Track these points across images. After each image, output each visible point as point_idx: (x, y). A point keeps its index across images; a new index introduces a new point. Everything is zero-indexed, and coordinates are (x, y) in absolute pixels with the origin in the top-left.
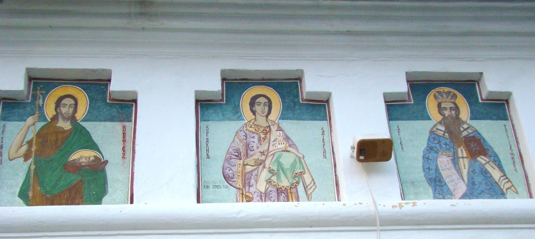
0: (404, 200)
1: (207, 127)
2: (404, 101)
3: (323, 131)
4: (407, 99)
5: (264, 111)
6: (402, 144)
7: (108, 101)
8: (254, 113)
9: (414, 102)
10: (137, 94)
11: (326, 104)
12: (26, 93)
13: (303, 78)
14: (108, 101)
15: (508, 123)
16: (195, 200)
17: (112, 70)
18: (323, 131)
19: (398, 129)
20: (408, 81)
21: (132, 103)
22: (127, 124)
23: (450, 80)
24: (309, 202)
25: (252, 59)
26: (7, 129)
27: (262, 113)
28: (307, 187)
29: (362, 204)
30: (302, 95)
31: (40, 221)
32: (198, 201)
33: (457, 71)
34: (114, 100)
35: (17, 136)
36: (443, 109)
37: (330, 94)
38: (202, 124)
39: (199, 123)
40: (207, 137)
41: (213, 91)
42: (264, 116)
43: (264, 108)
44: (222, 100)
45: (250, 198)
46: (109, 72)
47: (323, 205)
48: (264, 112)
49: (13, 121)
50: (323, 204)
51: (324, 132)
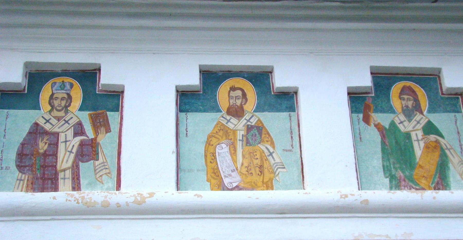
0: (361, 190)
1: (7, 113)
3: (187, 116)
7: (97, 93)
12: (199, 85)
13: (441, 71)
14: (97, 93)
18: (7, 115)
19: (358, 119)
20: (372, 73)
22: (292, 113)
25: (347, 55)
26: (71, 114)
28: (96, 167)
29: (310, 194)
35: (419, 126)
36: (402, 98)
40: (187, 123)
41: (10, 83)
47: (298, 194)
50: (299, 193)
51: (359, 119)
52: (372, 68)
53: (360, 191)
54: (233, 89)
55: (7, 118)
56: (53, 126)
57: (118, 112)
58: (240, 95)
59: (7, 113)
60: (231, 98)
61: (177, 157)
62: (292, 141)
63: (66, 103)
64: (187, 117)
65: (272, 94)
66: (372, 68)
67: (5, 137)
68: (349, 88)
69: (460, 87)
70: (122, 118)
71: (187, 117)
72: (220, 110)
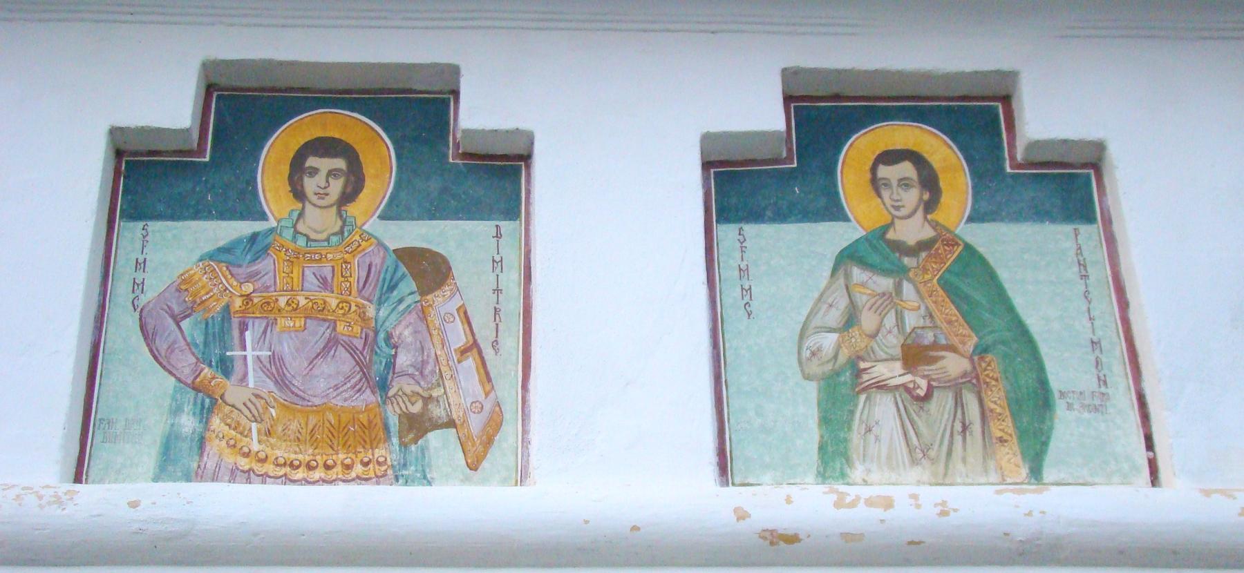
1: (143, 229)
2: (776, 161)
4: (784, 155)
5: (328, 190)
6: (1090, 296)
7: (795, 165)
8: (299, 194)
9: (211, 157)
10: (534, 138)
11: (523, 163)
12: (195, 135)
14: (795, 165)
15: (1090, 233)
16: (711, 469)
17: (463, 72)
21: (1087, 171)
22: (506, 226)
23: (929, 95)
24: (378, 486)
27: (316, 197)
30: (1012, 145)
31: (255, 535)
32: (78, 479)
33: (312, 59)
34: (468, 156)
37: (530, 138)
38: (130, 233)
39: (114, 222)
42: (331, 206)
43: (327, 181)
44: (201, 151)
45: (358, 469)
46: (453, 72)
48: (327, 195)
49: (186, 220)
52: (789, 75)
53: (519, 487)
54: (890, 157)
55: (744, 249)
56: (228, 289)
57: (1096, 226)
58: (907, 175)
59: (143, 229)
60: (883, 184)
61: (714, 362)
62: (497, 325)
63: (345, 186)
64: (742, 243)
65: (451, 160)
66: (789, 75)
67: (497, 316)
68: (708, 140)
69: (916, 152)
70: (1111, 241)
71: (742, 243)
72: (264, 213)
